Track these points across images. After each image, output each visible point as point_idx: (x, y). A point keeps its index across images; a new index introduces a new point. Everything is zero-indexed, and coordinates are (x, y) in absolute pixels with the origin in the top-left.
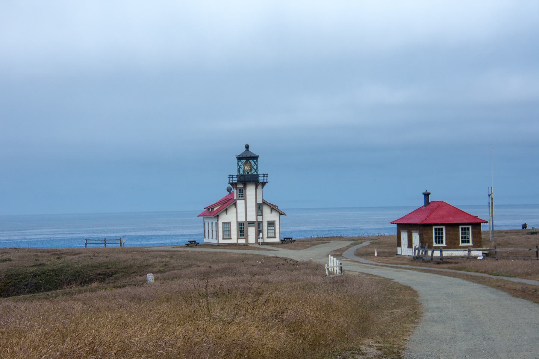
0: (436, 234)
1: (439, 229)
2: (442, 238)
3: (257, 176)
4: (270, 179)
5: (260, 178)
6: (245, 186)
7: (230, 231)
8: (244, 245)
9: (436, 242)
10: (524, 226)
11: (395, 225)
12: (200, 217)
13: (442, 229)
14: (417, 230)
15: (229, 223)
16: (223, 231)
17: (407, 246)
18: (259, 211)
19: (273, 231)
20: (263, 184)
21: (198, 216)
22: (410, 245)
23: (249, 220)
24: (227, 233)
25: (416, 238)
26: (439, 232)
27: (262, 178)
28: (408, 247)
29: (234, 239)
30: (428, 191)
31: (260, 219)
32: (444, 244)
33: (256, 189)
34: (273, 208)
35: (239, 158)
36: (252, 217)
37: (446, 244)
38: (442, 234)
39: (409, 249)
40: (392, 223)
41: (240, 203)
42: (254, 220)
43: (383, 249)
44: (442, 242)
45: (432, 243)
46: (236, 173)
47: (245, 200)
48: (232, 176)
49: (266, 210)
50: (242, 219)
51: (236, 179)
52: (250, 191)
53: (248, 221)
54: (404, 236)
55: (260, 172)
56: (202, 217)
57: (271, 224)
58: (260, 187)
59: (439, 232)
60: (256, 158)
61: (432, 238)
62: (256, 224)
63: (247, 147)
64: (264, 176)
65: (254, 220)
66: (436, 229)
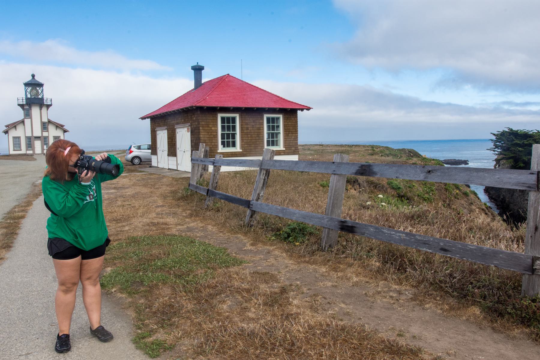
0: (223, 128)
1: (228, 118)
2: (234, 136)
3: (42, 99)
6: (30, 107)
8: (32, 155)
9: (223, 143)
11: (148, 121)
13: (234, 119)
14: (185, 122)
15: (19, 138)
16: (14, 144)
17: (166, 153)
18: (45, 126)
20: (48, 106)
22: (172, 151)
23: (35, 135)
25: (184, 136)
26: (229, 124)
28: (169, 155)
29: (23, 151)
30: (201, 64)
31: (45, 134)
32: (238, 149)
33: (41, 110)
34: (59, 126)
35: (27, 85)
36: (38, 132)
37: (242, 147)
38: (234, 128)
39: (171, 158)
40: (143, 118)
41: (27, 121)
42: (39, 134)
43: (530, 191)
44: (234, 145)
45: (217, 146)
46: (24, 97)
47: (31, 118)
49: (51, 128)
50: (29, 134)
52: (35, 111)
54: (162, 136)
55: (45, 97)
58: (44, 109)
59: (229, 124)
60: (41, 85)
61: (216, 136)
62: (42, 138)
63: (33, 76)
65: (40, 135)
66: (223, 119)
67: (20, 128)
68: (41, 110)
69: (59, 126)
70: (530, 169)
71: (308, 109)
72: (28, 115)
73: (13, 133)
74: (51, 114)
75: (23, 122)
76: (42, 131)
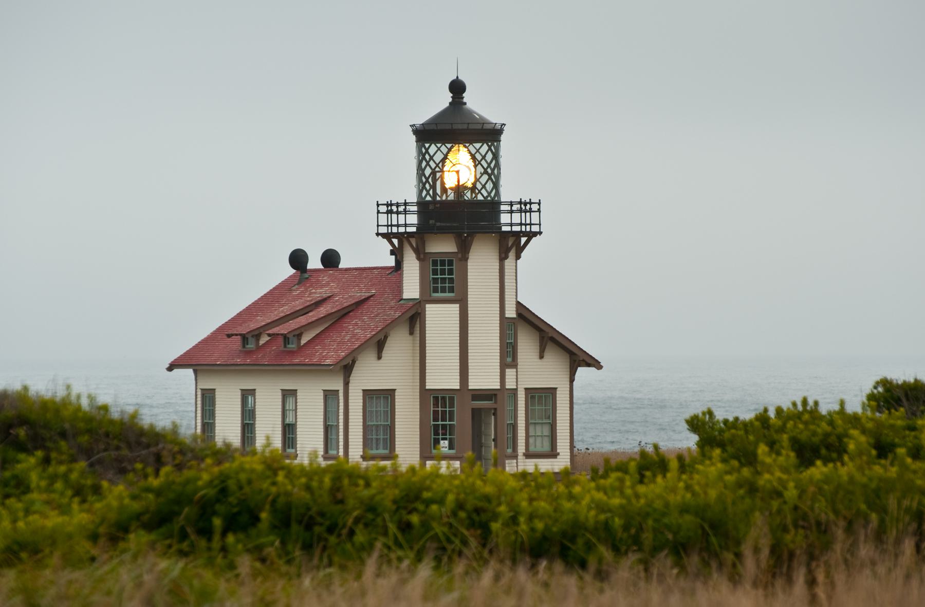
3: (492, 207)
4: (548, 219)
5: (505, 218)
7: (391, 428)
10: (298, 259)
12: (176, 371)
15: (389, 395)
19: (546, 431)
20: (511, 244)
21: (171, 368)
24: (380, 434)
27: (516, 218)
33: (503, 258)
36: (484, 377)
41: (440, 318)
46: (413, 198)
48: (391, 208)
50: (443, 377)
51: (413, 219)
53: (473, 384)
56: (190, 372)
57: (542, 398)
60: (490, 135)
63: (457, 88)
64: (525, 207)
67: (400, 346)
68: (503, 258)
69: (550, 339)
70: (553, 391)
71: (597, 364)
72: (446, 281)
73: (371, 374)
74: (541, 281)
75: (414, 319)
76: (504, 366)
